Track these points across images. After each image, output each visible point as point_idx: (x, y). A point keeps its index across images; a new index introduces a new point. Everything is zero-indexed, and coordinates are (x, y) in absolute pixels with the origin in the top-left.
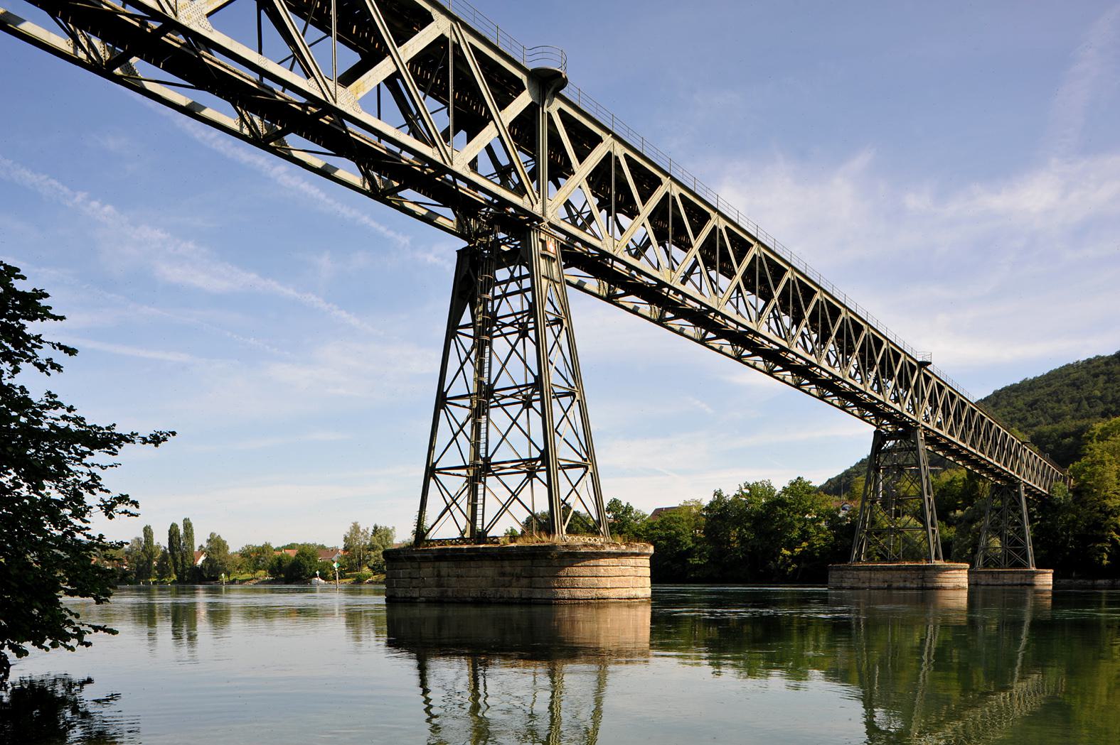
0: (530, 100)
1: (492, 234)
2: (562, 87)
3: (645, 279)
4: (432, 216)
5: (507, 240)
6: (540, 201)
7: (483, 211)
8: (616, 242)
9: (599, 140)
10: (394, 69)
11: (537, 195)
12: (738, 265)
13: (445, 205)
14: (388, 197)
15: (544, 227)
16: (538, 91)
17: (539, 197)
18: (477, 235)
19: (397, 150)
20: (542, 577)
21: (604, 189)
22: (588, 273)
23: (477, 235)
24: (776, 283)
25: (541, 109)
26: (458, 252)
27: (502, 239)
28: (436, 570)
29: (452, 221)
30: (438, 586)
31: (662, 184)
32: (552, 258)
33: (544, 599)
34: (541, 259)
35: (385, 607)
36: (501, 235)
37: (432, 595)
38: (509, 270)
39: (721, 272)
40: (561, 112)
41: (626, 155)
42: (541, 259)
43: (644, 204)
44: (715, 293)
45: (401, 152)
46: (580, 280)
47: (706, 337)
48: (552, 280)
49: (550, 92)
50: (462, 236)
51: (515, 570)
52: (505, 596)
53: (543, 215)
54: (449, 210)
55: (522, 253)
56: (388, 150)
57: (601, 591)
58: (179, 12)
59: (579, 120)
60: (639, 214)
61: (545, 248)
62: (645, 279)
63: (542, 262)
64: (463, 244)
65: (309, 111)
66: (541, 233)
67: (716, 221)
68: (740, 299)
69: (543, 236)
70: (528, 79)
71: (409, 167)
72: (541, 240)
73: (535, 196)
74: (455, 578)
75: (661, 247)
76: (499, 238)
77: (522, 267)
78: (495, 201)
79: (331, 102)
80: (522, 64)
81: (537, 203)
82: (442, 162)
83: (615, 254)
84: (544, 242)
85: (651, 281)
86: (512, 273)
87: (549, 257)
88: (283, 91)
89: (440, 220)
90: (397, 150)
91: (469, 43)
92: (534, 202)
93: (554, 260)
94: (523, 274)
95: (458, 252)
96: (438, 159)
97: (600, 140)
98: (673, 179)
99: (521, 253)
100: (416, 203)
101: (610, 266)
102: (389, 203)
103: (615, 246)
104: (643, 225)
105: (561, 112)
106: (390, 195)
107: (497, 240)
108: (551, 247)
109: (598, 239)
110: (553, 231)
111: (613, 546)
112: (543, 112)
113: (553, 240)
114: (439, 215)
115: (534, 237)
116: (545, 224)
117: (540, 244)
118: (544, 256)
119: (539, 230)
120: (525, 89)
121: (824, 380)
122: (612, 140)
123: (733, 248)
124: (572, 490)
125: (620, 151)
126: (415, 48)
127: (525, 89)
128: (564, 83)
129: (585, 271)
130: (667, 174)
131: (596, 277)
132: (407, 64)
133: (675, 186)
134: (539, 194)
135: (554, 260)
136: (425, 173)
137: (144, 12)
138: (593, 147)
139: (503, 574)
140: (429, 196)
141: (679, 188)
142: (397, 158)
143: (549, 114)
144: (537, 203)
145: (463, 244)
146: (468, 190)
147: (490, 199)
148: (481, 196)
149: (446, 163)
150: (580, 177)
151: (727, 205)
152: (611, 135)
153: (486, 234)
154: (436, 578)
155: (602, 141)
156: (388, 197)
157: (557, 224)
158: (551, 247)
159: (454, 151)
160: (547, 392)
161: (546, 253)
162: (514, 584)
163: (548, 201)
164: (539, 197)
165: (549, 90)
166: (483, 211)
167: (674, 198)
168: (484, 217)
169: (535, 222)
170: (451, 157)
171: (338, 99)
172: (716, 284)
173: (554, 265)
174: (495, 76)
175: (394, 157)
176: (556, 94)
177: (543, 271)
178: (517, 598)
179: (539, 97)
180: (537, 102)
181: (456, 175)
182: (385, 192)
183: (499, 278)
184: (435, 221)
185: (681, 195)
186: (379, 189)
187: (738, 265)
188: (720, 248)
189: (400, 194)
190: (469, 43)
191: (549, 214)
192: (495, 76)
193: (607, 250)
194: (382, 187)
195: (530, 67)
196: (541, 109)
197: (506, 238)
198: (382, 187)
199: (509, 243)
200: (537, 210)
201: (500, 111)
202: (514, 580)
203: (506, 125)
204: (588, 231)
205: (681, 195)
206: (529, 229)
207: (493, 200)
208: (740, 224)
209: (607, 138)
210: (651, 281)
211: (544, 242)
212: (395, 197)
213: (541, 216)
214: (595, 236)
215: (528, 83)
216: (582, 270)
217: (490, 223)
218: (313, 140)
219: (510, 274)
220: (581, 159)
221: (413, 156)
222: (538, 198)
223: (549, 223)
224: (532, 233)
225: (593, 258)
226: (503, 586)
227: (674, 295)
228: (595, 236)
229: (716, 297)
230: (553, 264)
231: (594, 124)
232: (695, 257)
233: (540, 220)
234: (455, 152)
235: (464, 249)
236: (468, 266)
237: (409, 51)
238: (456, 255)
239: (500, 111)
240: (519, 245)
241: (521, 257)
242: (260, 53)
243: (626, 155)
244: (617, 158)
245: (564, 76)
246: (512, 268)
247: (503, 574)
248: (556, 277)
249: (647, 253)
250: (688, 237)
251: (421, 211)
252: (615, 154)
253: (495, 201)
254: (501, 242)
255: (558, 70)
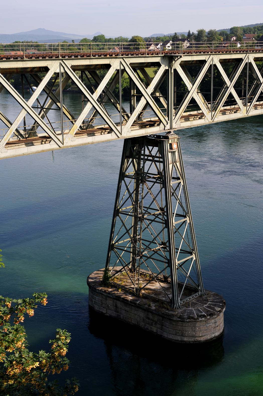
6: (169, 122)
7: (198, 62)
20: (168, 328)
28: (115, 303)
30: (115, 311)
33: (169, 338)
35: (88, 315)
37: (112, 315)
47: (146, 69)
51: (154, 318)
52: (149, 329)
57: (197, 338)
74: (124, 311)
111: (203, 318)
124: (178, 229)
134: (169, 118)
139: (148, 318)
154: (115, 307)
160: (171, 230)
162: (154, 325)
164: (169, 120)
166: (198, 62)
178: (155, 332)
201: (59, 73)
202: (154, 323)
222: (167, 121)
226: (148, 324)
239: (59, 73)
247: (148, 318)
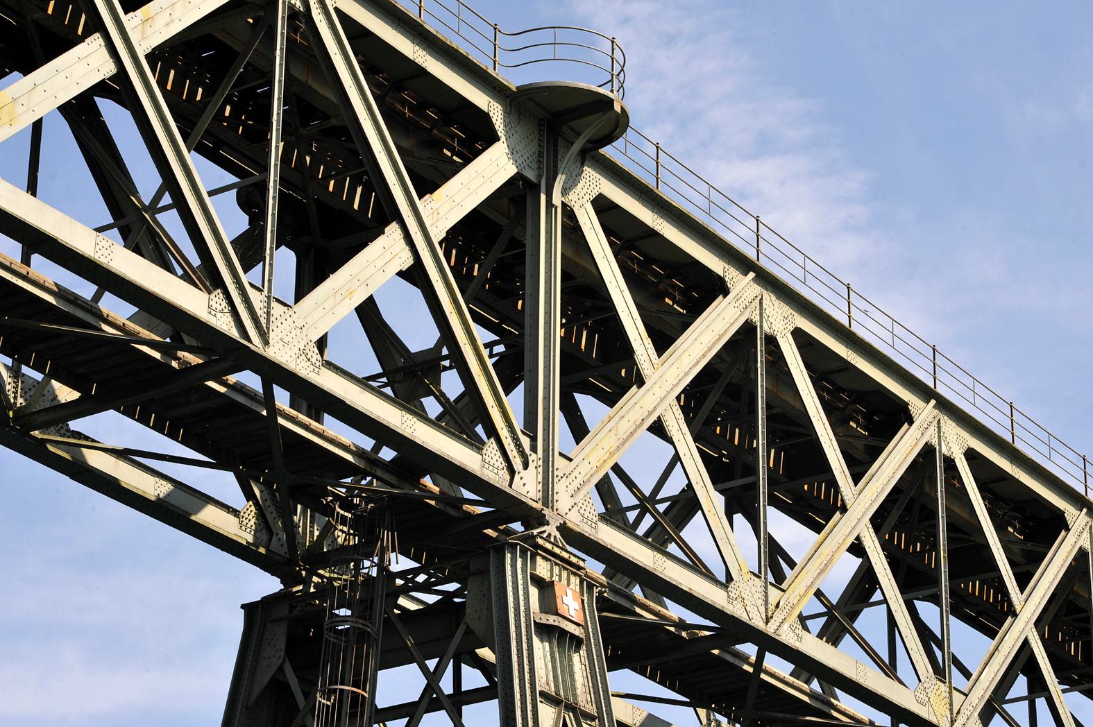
0: (510, 170)
1: (369, 556)
2: (609, 139)
3: (675, 611)
4: (183, 501)
5: (421, 578)
8: (957, 697)
9: (717, 288)
10: (109, 69)
11: (526, 442)
12: (1023, 582)
13: (221, 464)
14: (36, 433)
15: (547, 539)
16: (534, 147)
17: (534, 449)
18: (316, 558)
19: (85, 289)
21: (724, 430)
22: (672, 688)
23: (316, 558)
24: (858, 469)
25: (543, 197)
26: (249, 609)
27: (402, 574)
29: (235, 513)
31: (911, 422)
32: (573, 636)
34: (536, 640)
36: (400, 563)
38: (424, 669)
39: (956, 611)
40: (603, 206)
41: (798, 334)
42: (536, 640)
43: (856, 478)
44: (939, 672)
45: (97, 297)
46: (650, 716)
48: (572, 708)
49: (578, 145)
50: (267, 564)
53: (546, 504)
54: (229, 478)
55: (472, 618)
56: (61, 293)
58: (272, 335)
59: (658, 228)
60: (1015, 615)
61: (549, 601)
62: (675, 611)
63: (541, 649)
64: (270, 584)
65: (179, 359)
66: (539, 560)
67: (932, 430)
68: (1041, 703)
69: (543, 569)
70: (507, 113)
71: (123, 347)
72: (538, 581)
73: (519, 446)
75: (738, 518)
76: (394, 568)
77: (464, 667)
78: (387, 454)
79: (256, 342)
80: (491, 71)
81: (526, 466)
82: (234, 333)
83: (770, 630)
84: (545, 587)
85: (692, 618)
86: (433, 678)
87: (563, 633)
88: (26, 260)
89: (209, 516)
90: (85, 289)
91: (336, 9)
92: (517, 463)
93: (576, 642)
94: (464, 688)
95: (249, 609)
96: (224, 324)
97: (718, 288)
98: (945, 406)
99: (468, 618)
100: (124, 454)
101: (751, 670)
102: (38, 452)
103: (771, 607)
104: (658, 429)
105: (603, 206)
106: (42, 427)
107: (387, 575)
108: (571, 601)
109: (708, 575)
110: (573, 554)
112: (550, 204)
113: (575, 581)
114: (209, 500)
115: (514, 568)
116: (551, 529)
117: (534, 592)
118: (546, 631)
119: (533, 549)
120: (498, 139)
121: (111, 340)
122: (756, 289)
123: (1000, 528)
125: (955, 442)
126: (175, 16)
127: (498, 139)
128: (617, 125)
129: (662, 683)
130: (927, 393)
131: (694, 704)
132: (440, 243)
133: (951, 429)
134: (534, 439)
135: (576, 642)
136: (175, 364)
137: (479, 496)
138: (696, 308)
140: (172, 435)
141: (965, 435)
142: (90, 319)
143: (569, 213)
144: (526, 466)
145: (270, 584)
146: (294, 413)
147: (367, 443)
148: (346, 440)
149: (249, 340)
150: (659, 392)
151: (1044, 437)
152: (933, 402)
153: (341, 556)
155: (725, 291)
156: (36, 433)
157: (586, 530)
158: (571, 601)
159: (274, 304)
161: (552, 620)
163: (559, 462)
164: (534, 449)
165: (569, 148)
167: (950, 463)
168: (346, 504)
169: (517, 526)
170: (263, 321)
171: (273, 337)
172: (941, 648)
173: (578, 661)
174: (404, 103)
175: (80, 314)
176: (591, 155)
177: (544, 676)
179: (539, 162)
180: (531, 175)
181: (274, 373)
182: (26, 419)
183: (384, 699)
184: (194, 518)
185: (971, 455)
186: (11, 406)
187: (1023, 582)
188: (950, 527)
189: (74, 425)
190: (336, 9)
191: (563, 501)
192: (404, 103)
193: (744, 617)
194: (20, 401)
195: (513, 80)
196: (543, 197)
197: (415, 572)
198: (20, 401)
199: (426, 588)
200: (527, 486)
201: (420, 197)
203: (438, 234)
204: (672, 548)
205: (971, 455)
206: (499, 548)
207: (377, 449)
208: (1019, 445)
209: (742, 285)
210: (692, 618)
211: (545, 587)
212: (58, 433)
213: (538, 506)
214: (696, 565)
215: (507, 124)
216: (652, 678)
217: (366, 527)
218: (158, 428)
219: (423, 682)
220: (662, 341)
221: (793, 666)
223: (563, 529)
224: (508, 556)
225: (696, 640)
227: (792, 679)
228: (696, 565)
229: (944, 688)
230: (576, 658)
231: (984, 427)
232: (857, 548)
233: (534, 518)
234: (277, 309)
235: (268, 601)
236: (282, 653)
237: (160, 22)
238: (236, 625)
239: (420, 197)
240: (456, 593)
241: (469, 631)
242: (32, 188)
243: (798, 334)
244: (771, 341)
245: (617, 108)
246: (432, 664)
248: (585, 700)
249: (859, 624)
250: (833, 484)
251: (152, 488)
252: (944, 450)
253: (387, 454)
254: (399, 582)
255: (601, 90)
